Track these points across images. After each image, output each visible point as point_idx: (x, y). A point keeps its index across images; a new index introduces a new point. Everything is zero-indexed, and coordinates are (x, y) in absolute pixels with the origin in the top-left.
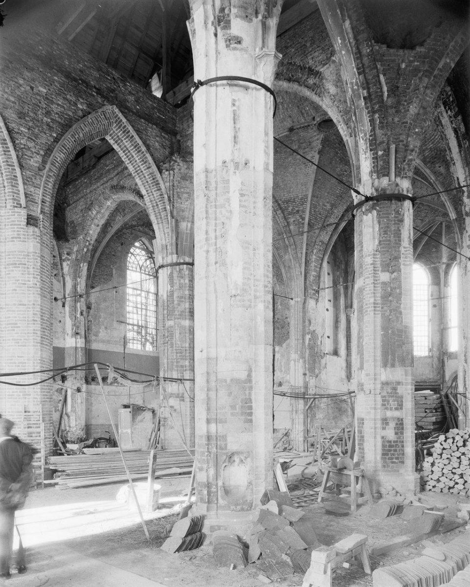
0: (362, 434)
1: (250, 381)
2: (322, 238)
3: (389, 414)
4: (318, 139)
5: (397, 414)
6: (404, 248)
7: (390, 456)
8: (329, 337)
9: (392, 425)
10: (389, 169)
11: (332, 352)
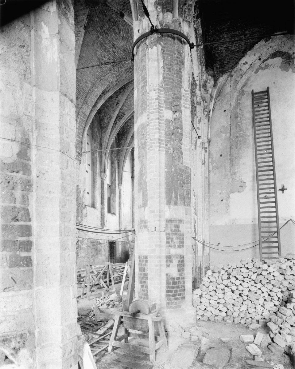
0: (146, 272)
1: (26, 169)
2: (84, 110)
3: (173, 251)
4: (84, 14)
5: (179, 251)
6: (185, 90)
7: (173, 293)
8: (88, 193)
9: (175, 262)
10: (173, 5)
11: (90, 205)
